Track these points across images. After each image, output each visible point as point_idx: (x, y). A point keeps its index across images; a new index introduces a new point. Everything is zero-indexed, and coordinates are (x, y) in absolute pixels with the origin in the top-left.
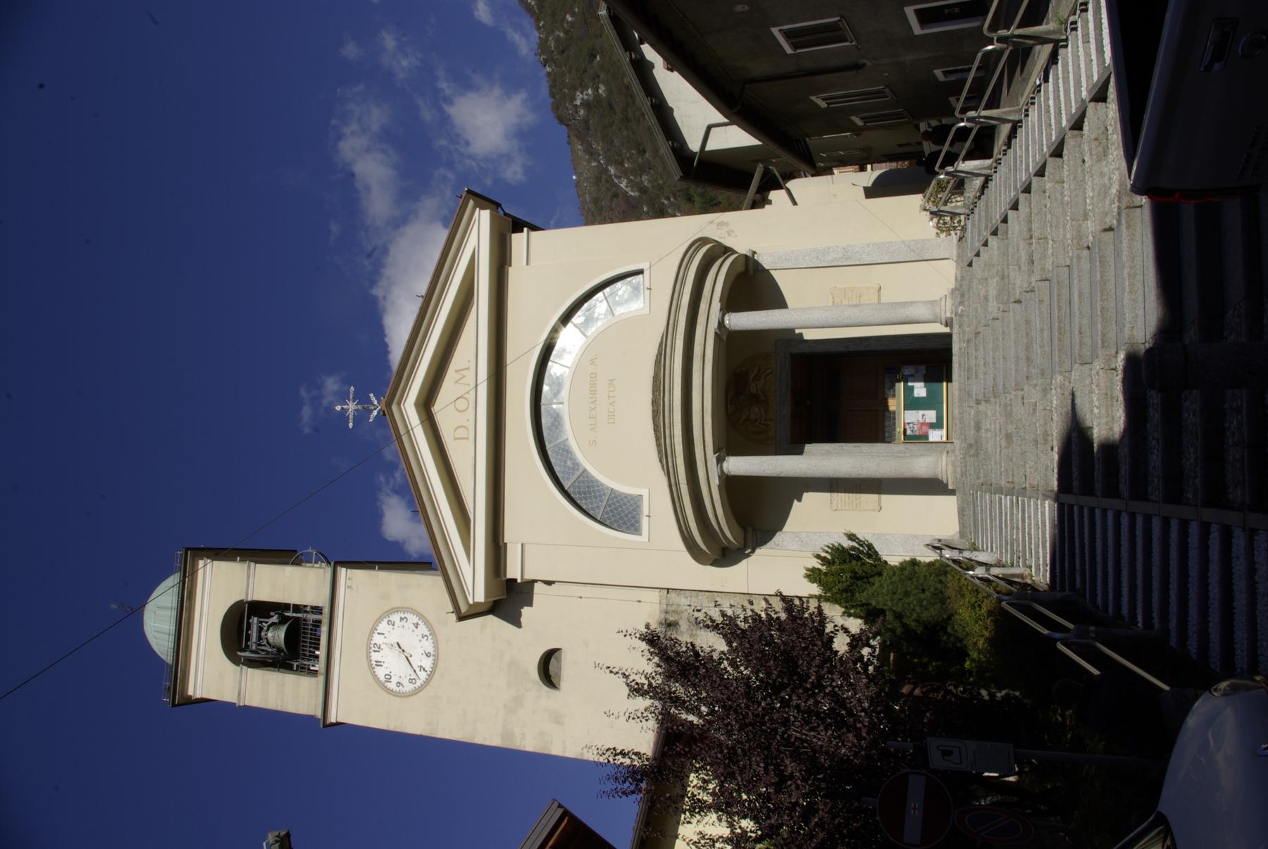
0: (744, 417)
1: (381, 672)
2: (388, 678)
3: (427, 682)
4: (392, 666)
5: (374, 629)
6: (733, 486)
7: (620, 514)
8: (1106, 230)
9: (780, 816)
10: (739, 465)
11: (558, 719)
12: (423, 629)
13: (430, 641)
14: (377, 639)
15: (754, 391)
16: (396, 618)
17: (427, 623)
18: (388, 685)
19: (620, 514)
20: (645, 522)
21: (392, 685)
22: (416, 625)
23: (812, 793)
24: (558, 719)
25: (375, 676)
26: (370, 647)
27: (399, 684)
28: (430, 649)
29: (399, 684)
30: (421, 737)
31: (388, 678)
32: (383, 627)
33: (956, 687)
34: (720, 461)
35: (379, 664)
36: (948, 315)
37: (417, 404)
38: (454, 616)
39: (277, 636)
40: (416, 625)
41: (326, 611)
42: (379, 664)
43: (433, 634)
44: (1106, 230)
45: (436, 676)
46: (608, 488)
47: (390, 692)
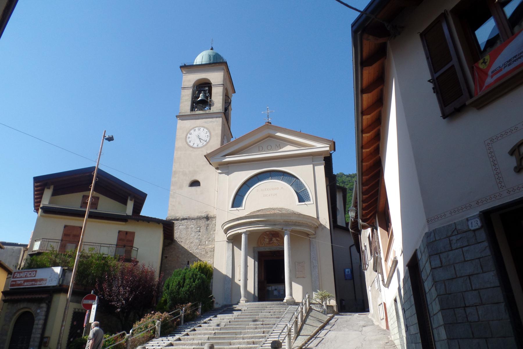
2: (191, 134)
3: (190, 146)
4: (194, 135)
7: (237, 201)
8: (188, 262)
10: (243, 236)
14: (202, 129)
16: (208, 134)
19: (237, 201)
20: (235, 209)
23: (127, 341)
26: (199, 127)
27: (189, 137)
29: (189, 137)
31: (191, 134)
32: (206, 130)
34: (244, 233)
35: (195, 130)
44: (188, 262)
45: (192, 149)
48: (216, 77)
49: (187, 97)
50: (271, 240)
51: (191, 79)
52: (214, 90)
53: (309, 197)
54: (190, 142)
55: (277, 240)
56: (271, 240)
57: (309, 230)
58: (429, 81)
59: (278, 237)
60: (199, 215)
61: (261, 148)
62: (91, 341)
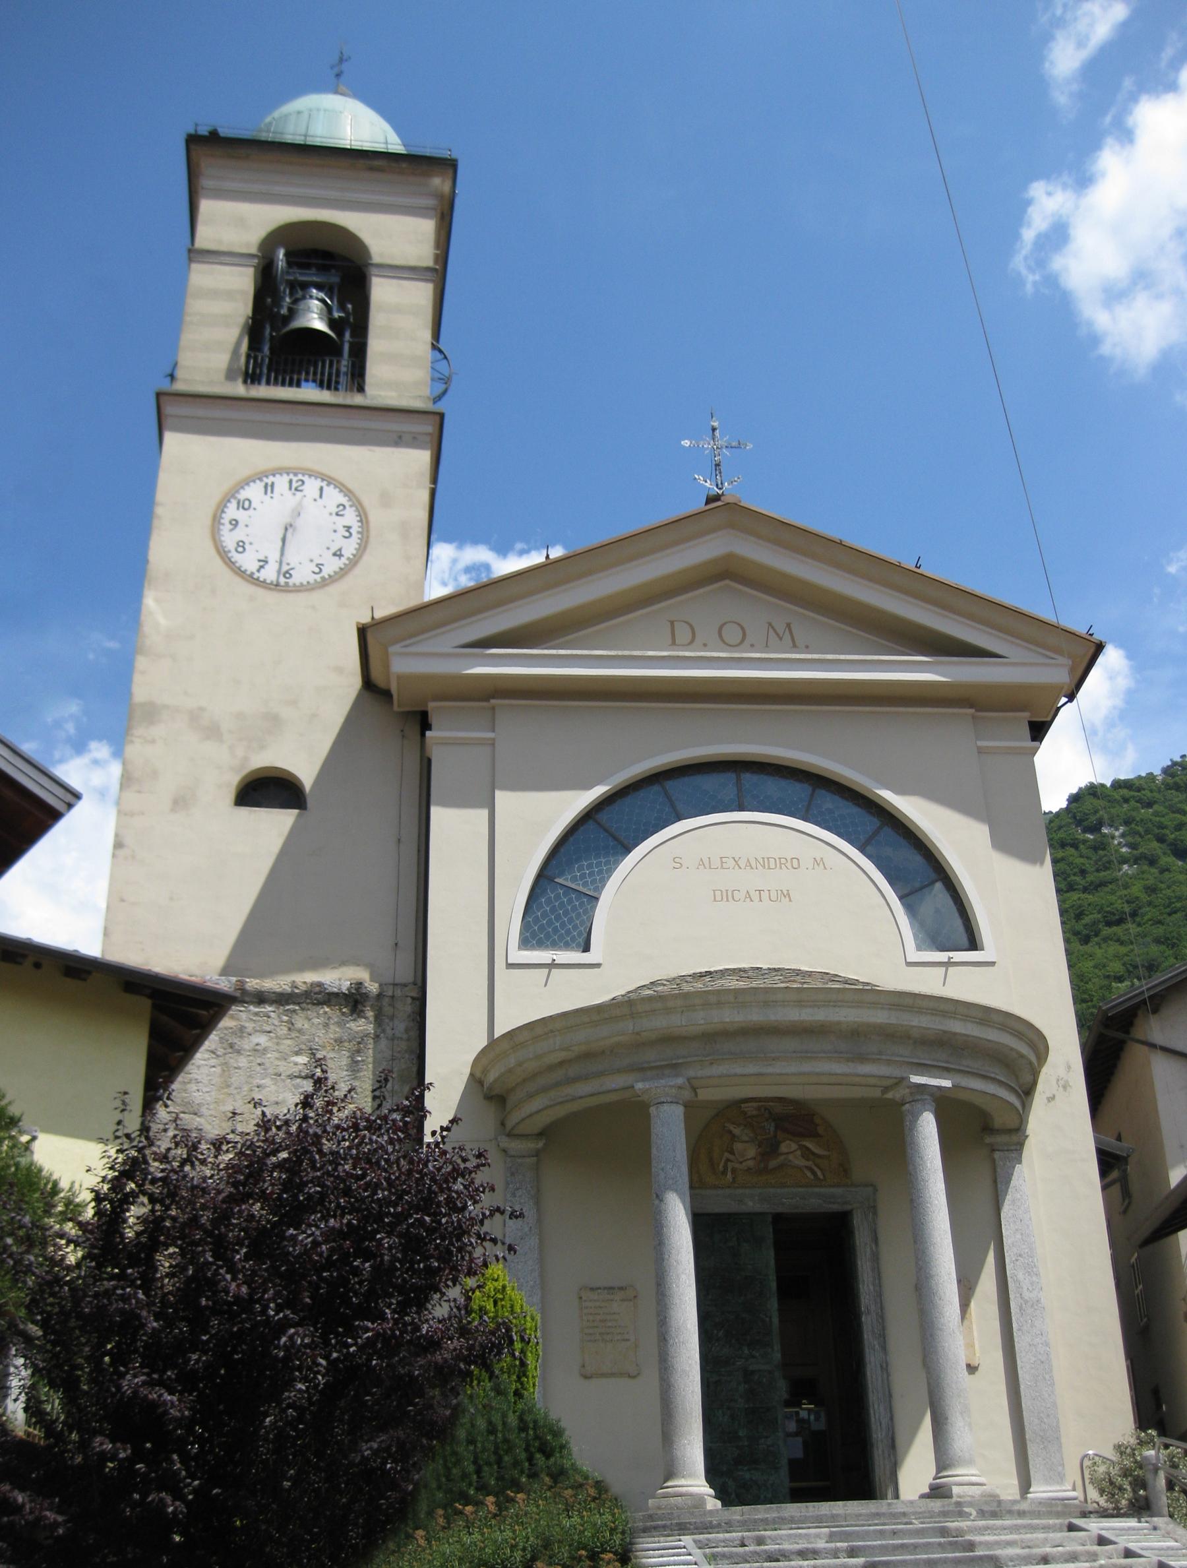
0: (737, 1131)
1: (253, 492)
3: (240, 572)
5: (330, 480)
6: (633, 1116)
9: (244, 1267)
11: (180, 803)
12: (332, 566)
13: (312, 578)
14: (312, 486)
15: (784, 1148)
16: (350, 517)
17: (343, 573)
18: (232, 505)
19: (559, 904)
21: (232, 511)
22: (338, 554)
24: (180, 803)
25: (247, 482)
27: (235, 523)
28: (297, 578)
29: (235, 523)
30: (147, 561)
32: (334, 497)
33: (162, 1504)
35: (269, 488)
36: (956, 1490)
37: (731, 556)
38: (366, 619)
39: (314, 317)
40: (338, 554)
41: (358, 399)
42: (269, 488)
43: (325, 583)
46: (599, 889)
47: (221, 508)
48: (393, 235)
49: (219, 303)
50: (770, 1149)
51: (240, 221)
52: (382, 291)
53: (532, 948)
54: (241, 546)
55: (807, 1153)
56: (770, 1149)
57: (991, 1088)
58: (559, 1421)
59: (813, 1135)
60: (957, 914)
61: (683, 634)
62: (178, 1414)
